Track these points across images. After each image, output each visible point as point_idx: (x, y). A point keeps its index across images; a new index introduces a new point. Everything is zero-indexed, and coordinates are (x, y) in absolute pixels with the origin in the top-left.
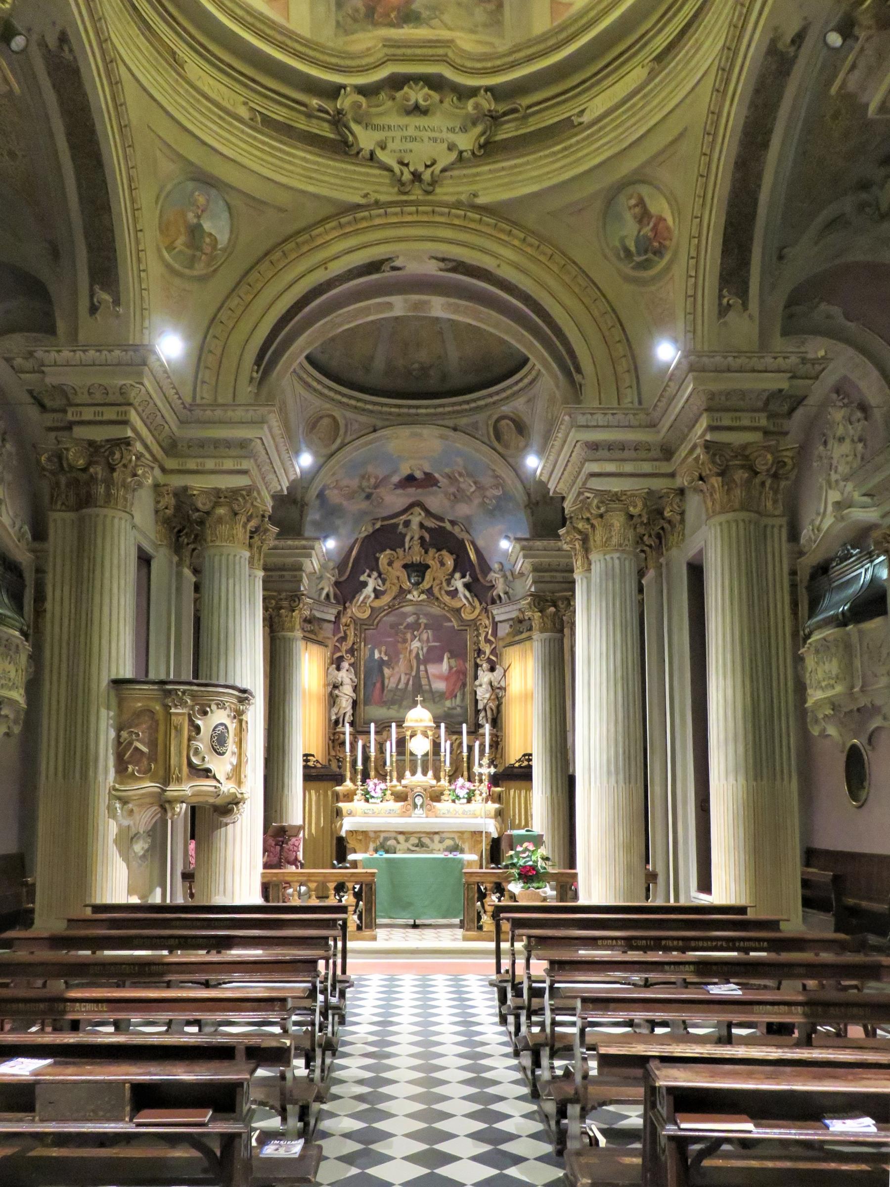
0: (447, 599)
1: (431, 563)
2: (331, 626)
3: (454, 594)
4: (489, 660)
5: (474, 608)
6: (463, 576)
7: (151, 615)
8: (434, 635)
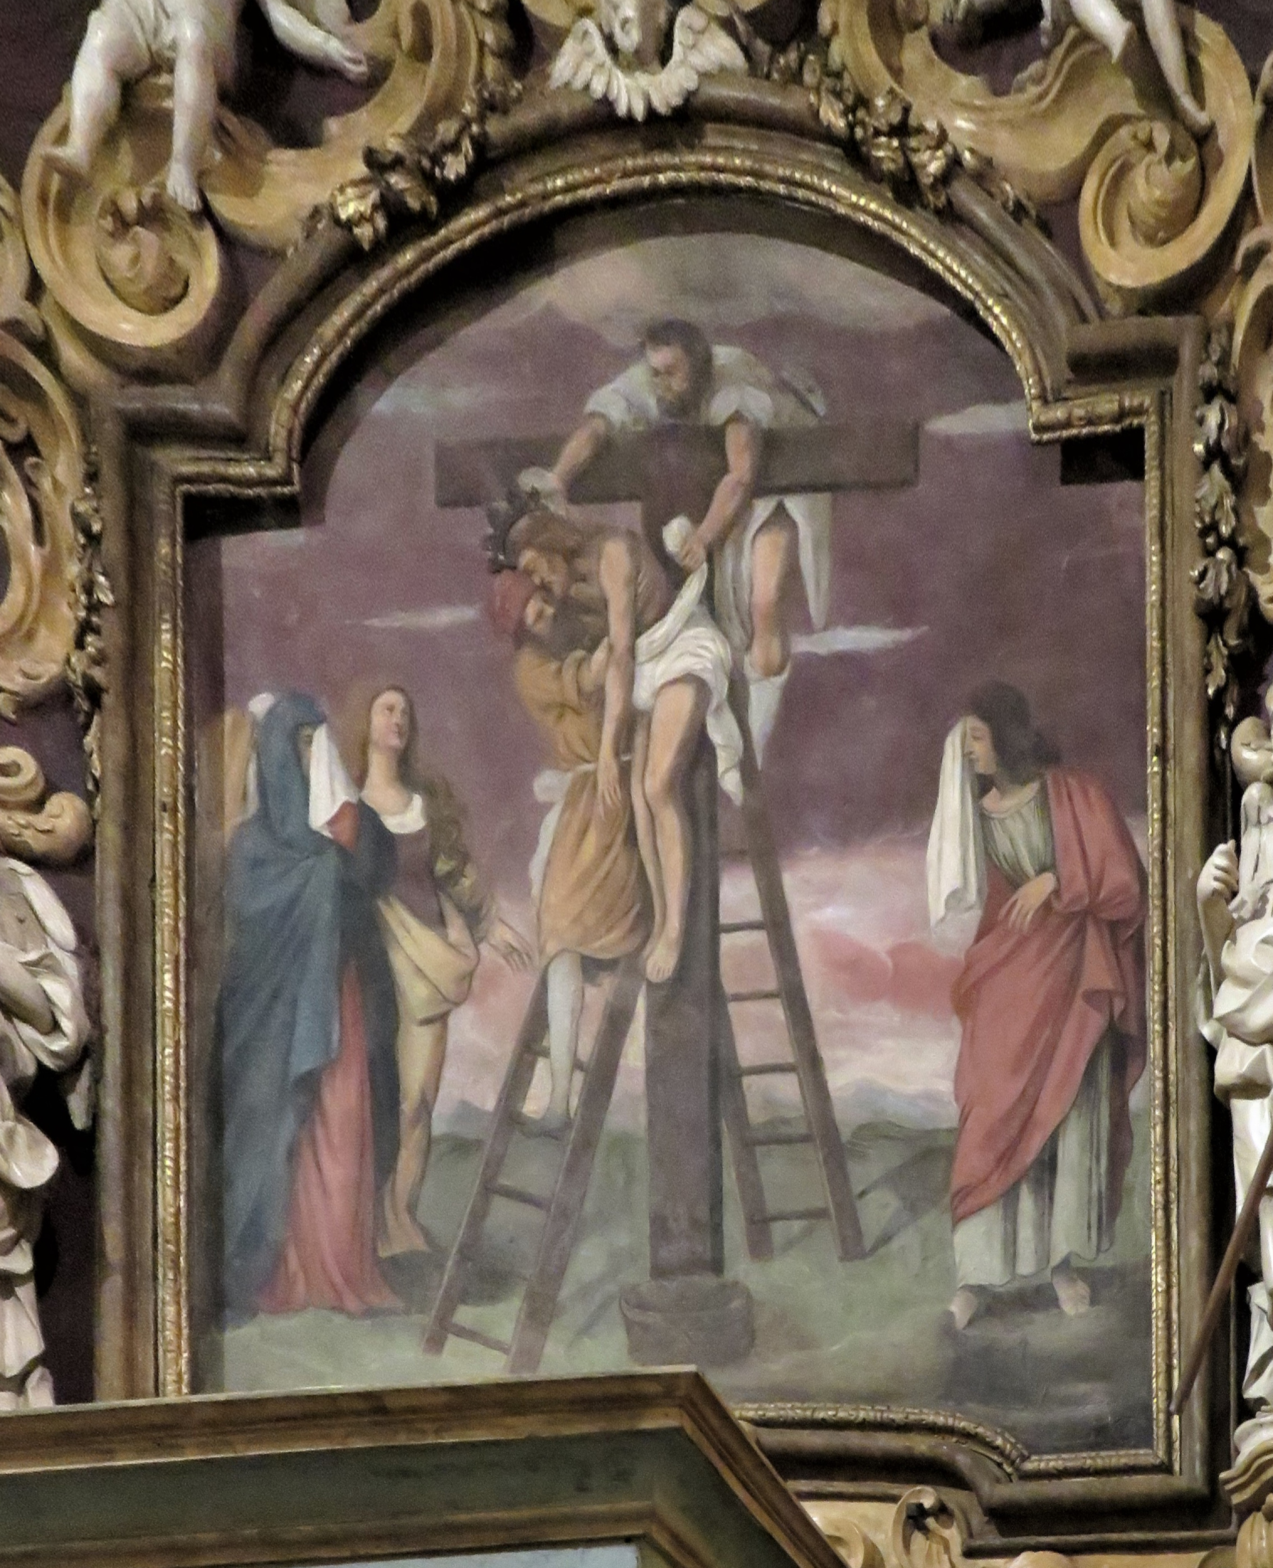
8: (847, 556)
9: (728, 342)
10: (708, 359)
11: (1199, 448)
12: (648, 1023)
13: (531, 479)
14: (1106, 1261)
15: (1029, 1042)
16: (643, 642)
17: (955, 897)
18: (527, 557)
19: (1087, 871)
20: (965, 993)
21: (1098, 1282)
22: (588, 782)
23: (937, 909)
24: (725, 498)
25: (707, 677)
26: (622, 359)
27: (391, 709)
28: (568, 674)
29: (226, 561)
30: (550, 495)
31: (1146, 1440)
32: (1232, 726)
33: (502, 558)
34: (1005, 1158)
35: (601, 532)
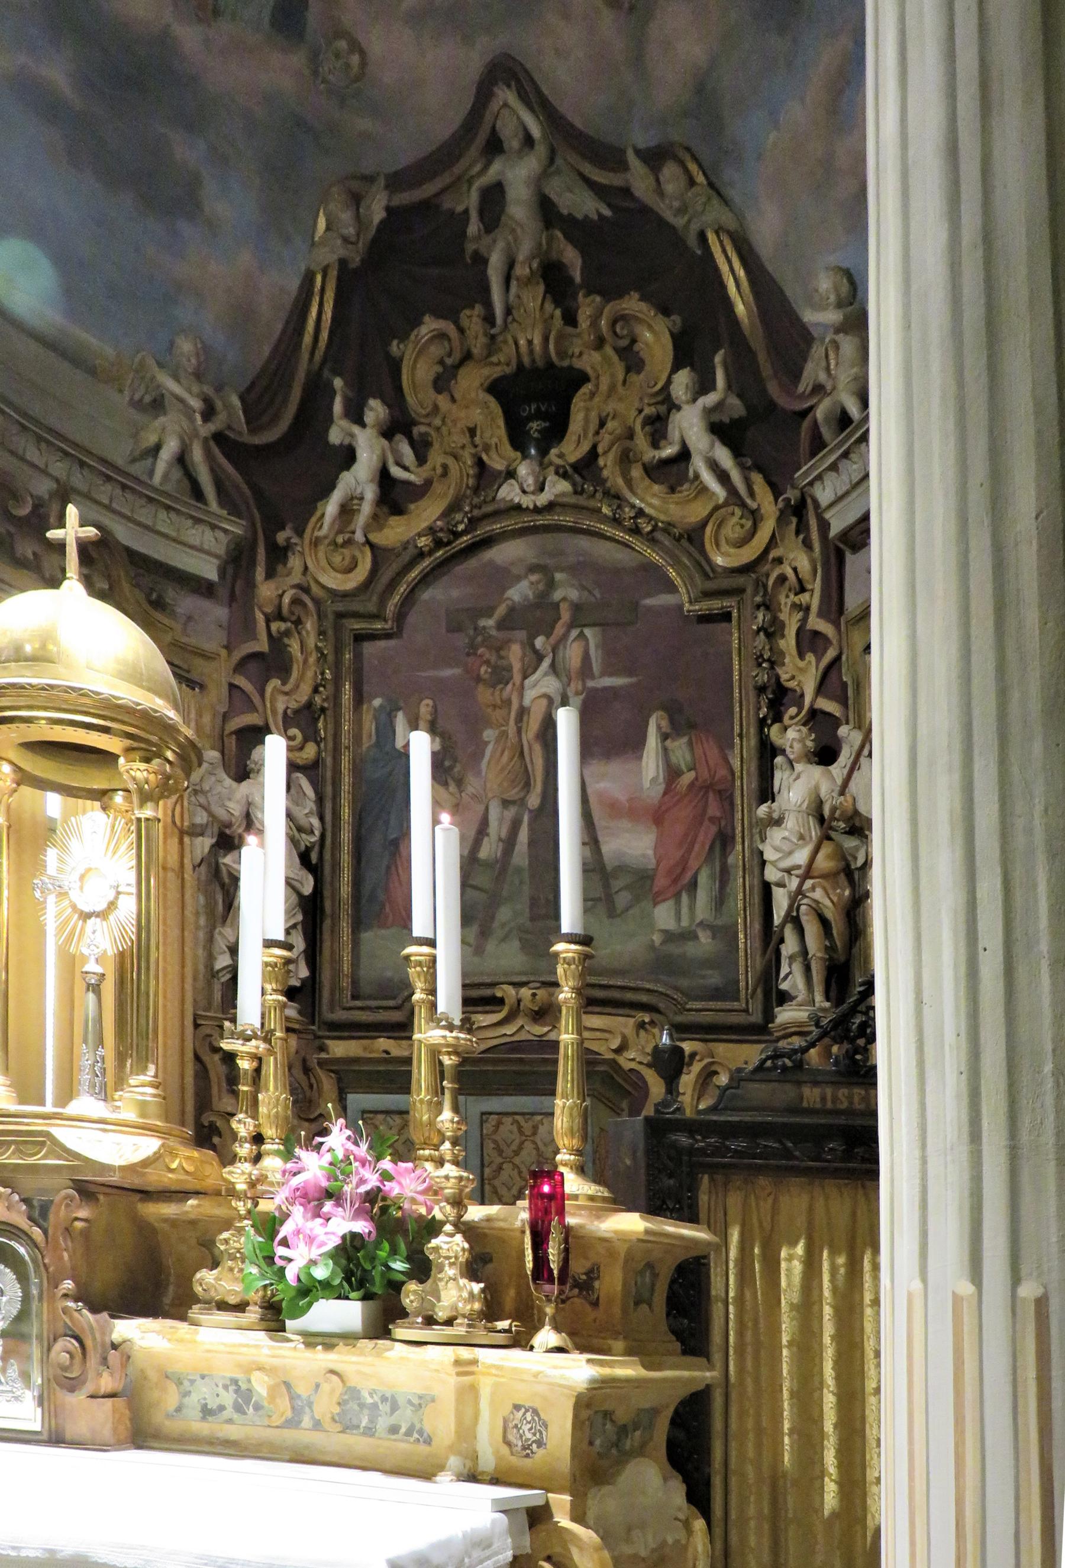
0: (651, 499)
1: (589, 361)
2: (220, 612)
3: (673, 471)
4: (814, 716)
5: (755, 516)
6: (704, 386)
7: (905, 1319)
8: (609, 651)
9: (562, 570)
10: (553, 578)
11: (755, 627)
12: (529, 825)
13: (482, 622)
14: (719, 922)
15: (686, 835)
16: (527, 682)
17: (654, 780)
18: (480, 651)
19: (709, 770)
20: (658, 817)
21: (715, 931)
22: (504, 734)
23: (646, 784)
24: (559, 630)
25: (552, 695)
26: (519, 579)
27: (428, 705)
28: (497, 693)
29: (365, 651)
30: (490, 627)
31: (738, 999)
32: (769, 726)
33: (472, 649)
34: (675, 881)
35: (509, 641)
